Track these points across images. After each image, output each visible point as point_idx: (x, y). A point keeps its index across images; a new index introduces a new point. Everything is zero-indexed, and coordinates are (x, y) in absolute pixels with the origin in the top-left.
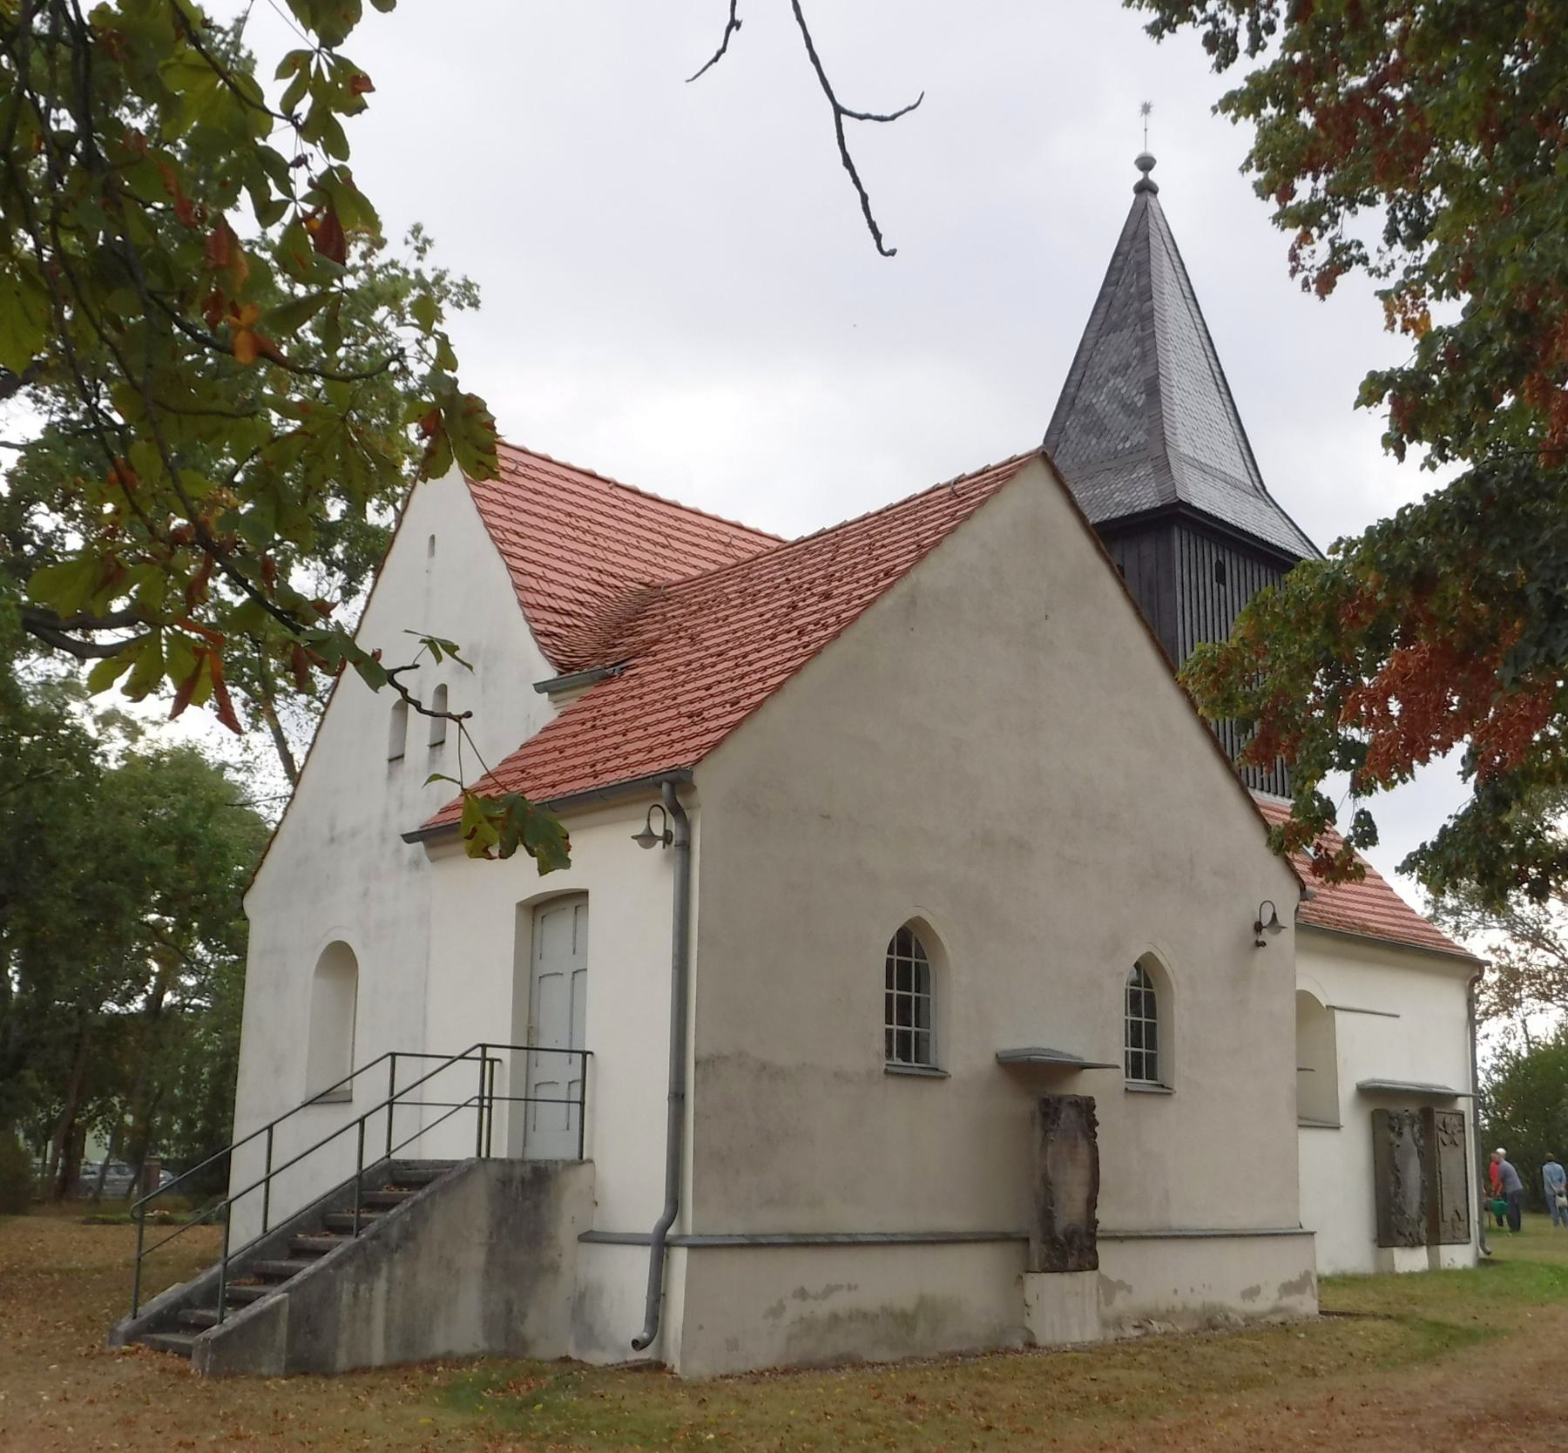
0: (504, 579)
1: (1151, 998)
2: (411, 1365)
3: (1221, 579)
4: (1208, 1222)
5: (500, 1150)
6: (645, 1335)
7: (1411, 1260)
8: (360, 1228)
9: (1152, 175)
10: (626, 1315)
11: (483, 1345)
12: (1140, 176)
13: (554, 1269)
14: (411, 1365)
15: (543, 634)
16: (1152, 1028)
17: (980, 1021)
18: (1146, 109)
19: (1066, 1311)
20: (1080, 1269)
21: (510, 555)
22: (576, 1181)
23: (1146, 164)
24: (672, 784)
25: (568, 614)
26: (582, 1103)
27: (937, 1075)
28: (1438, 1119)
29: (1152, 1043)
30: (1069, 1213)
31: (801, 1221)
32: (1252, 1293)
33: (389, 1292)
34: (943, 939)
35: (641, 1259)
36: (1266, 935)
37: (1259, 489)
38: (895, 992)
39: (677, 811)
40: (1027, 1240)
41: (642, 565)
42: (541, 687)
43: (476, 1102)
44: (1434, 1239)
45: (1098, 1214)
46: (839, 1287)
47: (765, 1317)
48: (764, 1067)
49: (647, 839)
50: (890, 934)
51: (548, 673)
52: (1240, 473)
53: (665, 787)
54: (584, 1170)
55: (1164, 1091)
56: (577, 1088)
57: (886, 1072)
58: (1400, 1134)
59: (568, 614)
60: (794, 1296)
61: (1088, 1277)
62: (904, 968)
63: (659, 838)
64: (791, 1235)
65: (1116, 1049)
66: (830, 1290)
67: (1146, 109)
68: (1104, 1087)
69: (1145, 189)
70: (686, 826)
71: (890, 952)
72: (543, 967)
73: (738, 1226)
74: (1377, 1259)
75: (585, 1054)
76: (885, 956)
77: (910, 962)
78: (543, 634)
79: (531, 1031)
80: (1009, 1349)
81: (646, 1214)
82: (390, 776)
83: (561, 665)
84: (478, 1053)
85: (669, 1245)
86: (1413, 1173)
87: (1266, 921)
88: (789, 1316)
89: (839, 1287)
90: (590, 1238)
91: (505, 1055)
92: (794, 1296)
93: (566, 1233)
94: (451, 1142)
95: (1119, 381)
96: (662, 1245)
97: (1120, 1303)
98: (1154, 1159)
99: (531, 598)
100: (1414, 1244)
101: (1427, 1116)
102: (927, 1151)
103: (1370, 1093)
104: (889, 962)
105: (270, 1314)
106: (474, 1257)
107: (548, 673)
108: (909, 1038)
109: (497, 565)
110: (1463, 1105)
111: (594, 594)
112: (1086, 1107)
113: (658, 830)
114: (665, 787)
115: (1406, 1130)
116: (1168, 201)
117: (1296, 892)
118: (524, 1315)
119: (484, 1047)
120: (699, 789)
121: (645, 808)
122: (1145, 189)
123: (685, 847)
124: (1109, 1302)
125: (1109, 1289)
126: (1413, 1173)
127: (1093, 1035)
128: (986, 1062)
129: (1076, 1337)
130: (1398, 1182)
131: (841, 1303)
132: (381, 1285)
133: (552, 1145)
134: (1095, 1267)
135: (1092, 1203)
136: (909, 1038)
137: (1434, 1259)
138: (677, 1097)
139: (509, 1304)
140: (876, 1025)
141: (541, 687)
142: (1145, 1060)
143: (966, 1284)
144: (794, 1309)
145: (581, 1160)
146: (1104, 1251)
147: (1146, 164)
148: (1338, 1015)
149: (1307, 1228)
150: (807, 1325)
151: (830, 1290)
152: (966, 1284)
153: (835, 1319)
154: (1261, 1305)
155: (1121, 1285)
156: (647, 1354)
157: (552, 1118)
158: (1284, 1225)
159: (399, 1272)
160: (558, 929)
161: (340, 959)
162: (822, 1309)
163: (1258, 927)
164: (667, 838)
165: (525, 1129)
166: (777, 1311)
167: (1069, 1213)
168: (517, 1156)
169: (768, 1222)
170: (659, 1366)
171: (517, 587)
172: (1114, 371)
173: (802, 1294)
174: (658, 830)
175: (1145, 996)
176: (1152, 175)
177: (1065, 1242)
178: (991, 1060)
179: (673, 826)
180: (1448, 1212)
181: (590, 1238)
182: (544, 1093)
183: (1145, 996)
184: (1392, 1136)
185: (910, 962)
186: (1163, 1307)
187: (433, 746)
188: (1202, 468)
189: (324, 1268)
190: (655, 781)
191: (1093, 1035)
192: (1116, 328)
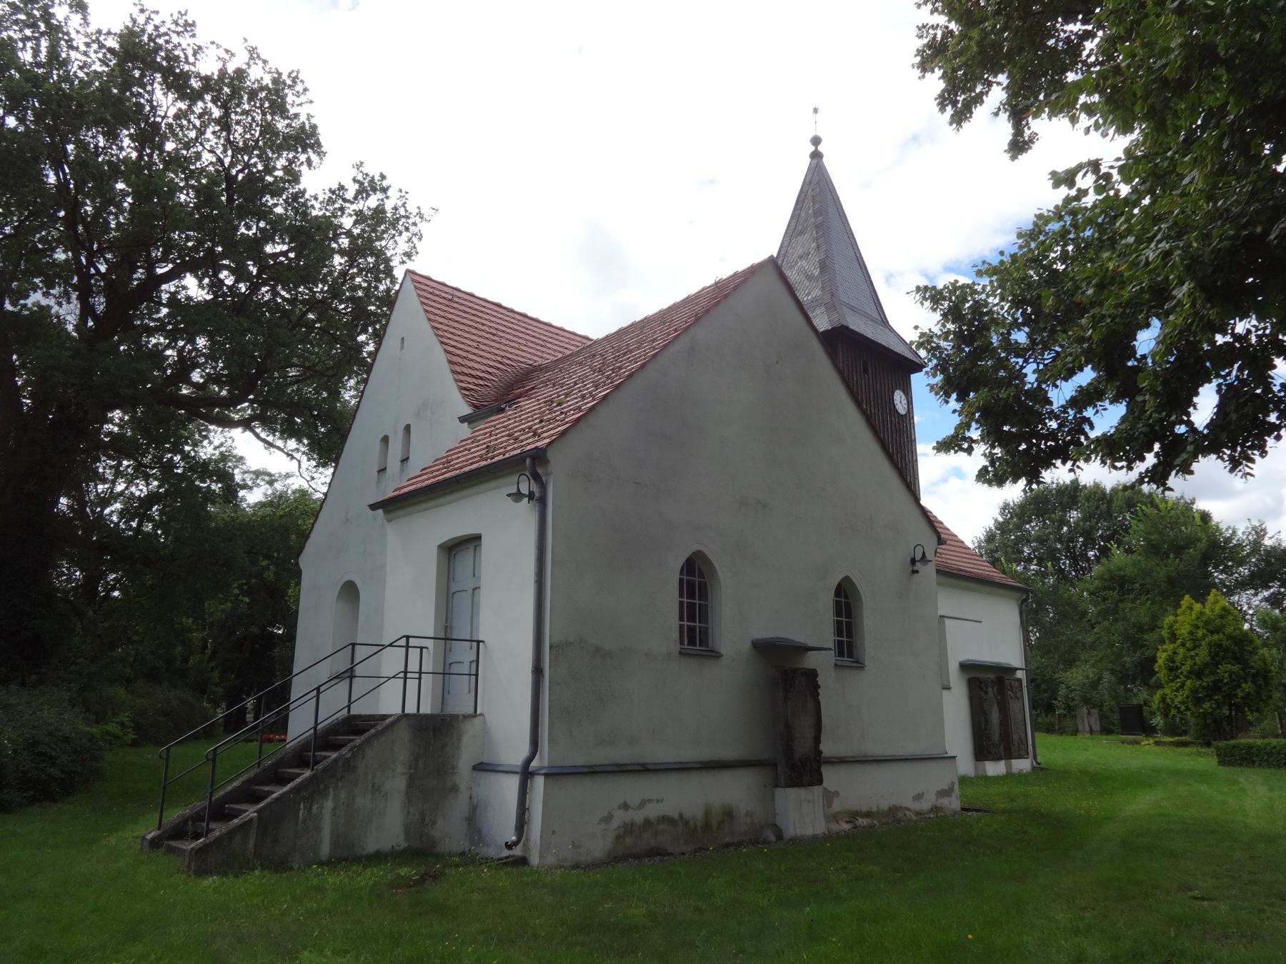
0: (443, 358)
1: (848, 606)
2: (347, 856)
3: (866, 371)
4: (872, 749)
5: (411, 709)
6: (514, 838)
7: (995, 768)
8: (316, 763)
9: (820, 148)
10: (502, 825)
11: (404, 845)
12: (813, 148)
13: (455, 789)
14: (347, 856)
15: (465, 389)
16: (849, 625)
17: (739, 622)
18: (816, 111)
19: (802, 814)
20: (812, 784)
21: (450, 353)
22: (471, 728)
23: (816, 141)
24: (533, 459)
25: (481, 378)
26: (477, 675)
27: (715, 655)
28: (1007, 682)
29: (850, 635)
30: (803, 747)
31: (622, 754)
32: (919, 797)
33: (334, 809)
34: (718, 568)
35: (511, 784)
36: (918, 566)
37: (885, 322)
38: (685, 623)
39: (536, 477)
40: (775, 765)
41: (528, 356)
42: (463, 419)
43: (402, 675)
44: (1009, 755)
45: (822, 747)
46: (650, 801)
47: (599, 823)
48: (598, 650)
49: (517, 496)
50: (680, 562)
51: (467, 410)
52: (875, 314)
53: (528, 461)
54: (477, 721)
55: (859, 665)
56: (474, 665)
57: (680, 653)
58: (986, 693)
59: (481, 378)
60: (620, 808)
61: (817, 790)
62: (691, 585)
63: (524, 496)
64: (617, 765)
65: (829, 639)
66: (643, 804)
67: (816, 111)
68: (823, 663)
69: (816, 156)
70: (543, 487)
71: (682, 573)
72: (454, 587)
73: (580, 760)
74: (976, 768)
75: (478, 642)
76: (678, 576)
77: (696, 580)
78: (465, 389)
79: (448, 627)
80: (765, 840)
81: (514, 749)
82: (379, 481)
83: (475, 406)
84: (403, 642)
85: (533, 774)
86: (995, 716)
87: (918, 557)
88: (616, 823)
89: (650, 801)
90: (482, 767)
91: (430, 643)
92: (620, 808)
93: (464, 763)
94: (388, 702)
95: (804, 263)
96: (526, 774)
97: (837, 806)
98: (853, 710)
99: (458, 369)
100: (999, 759)
101: (1000, 681)
102: (706, 707)
103: (965, 667)
104: (681, 581)
105: (245, 826)
106: (397, 783)
107: (467, 410)
108: (696, 637)
109: (439, 349)
110: (1020, 675)
111: (498, 369)
112: (812, 675)
113: (525, 491)
114: (528, 461)
115: (990, 690)
116: (826, 161)
117: (935, 540)
118: (434, 823)
119: (408, 637)
120: (552, 462)
121: (514, 478)
122: (816, 156)
123: (542, 501)
124: (829, 807)
125: (829, 796)
126: (995, 716)
127: (812, 628)
128: (746, 646)
129: (809, 831)
130: (986, 720)
131: (652, 811)
132: (329, 804)
133: (461, 705)
134: (820, 782)
135: (817, 740)
136: (696, 637)
137: (1009, 767)
138: (538, 671)
139: (423, 815)
140: (671, 620)
141: (463, 419)
142: (847, 646)
143: (735, 792)
144: (620, 817)
145: (475, 715)
146: (827, 772)
147: (816, 141)
148: (947, 620)
149: (950, 754)
150: (629, 829)
151: (643, 804)
152: (735, 792)
153: (647, 823)
154: (924, 805)
155: (837, 794)
156: (518, 851)
157: (461, 685)
158: (935, 752)
159: (343, 795)
160: (465, 558)
161: (350, 591)
162: (638, 817)
163: (913, 561)
164: (531, 496)
165: (444, 694)
166: (608, 818)
167: (803, 747)
168: (437, 711)
169: (602, 756)
170: (523, 861)
171: (450, 362)
172: (801, 257)
173: (625, 806)
174: (525, 491)
175: (846, 601)
176: (820, 148)
177: (799, 764)
178: (748, 645)
179: (535, 488)
180: (1015, 737)
181: (482, 767)
182: (455, 669)
183: (846, 601)
184: (982, 694)
185: (696, 580)
186: (864, 809)
187: (402, 461)
188: (853, 309)
189: (286, 793)
190: (521, 458)
191: (812, 628)
192: (802, 233)
